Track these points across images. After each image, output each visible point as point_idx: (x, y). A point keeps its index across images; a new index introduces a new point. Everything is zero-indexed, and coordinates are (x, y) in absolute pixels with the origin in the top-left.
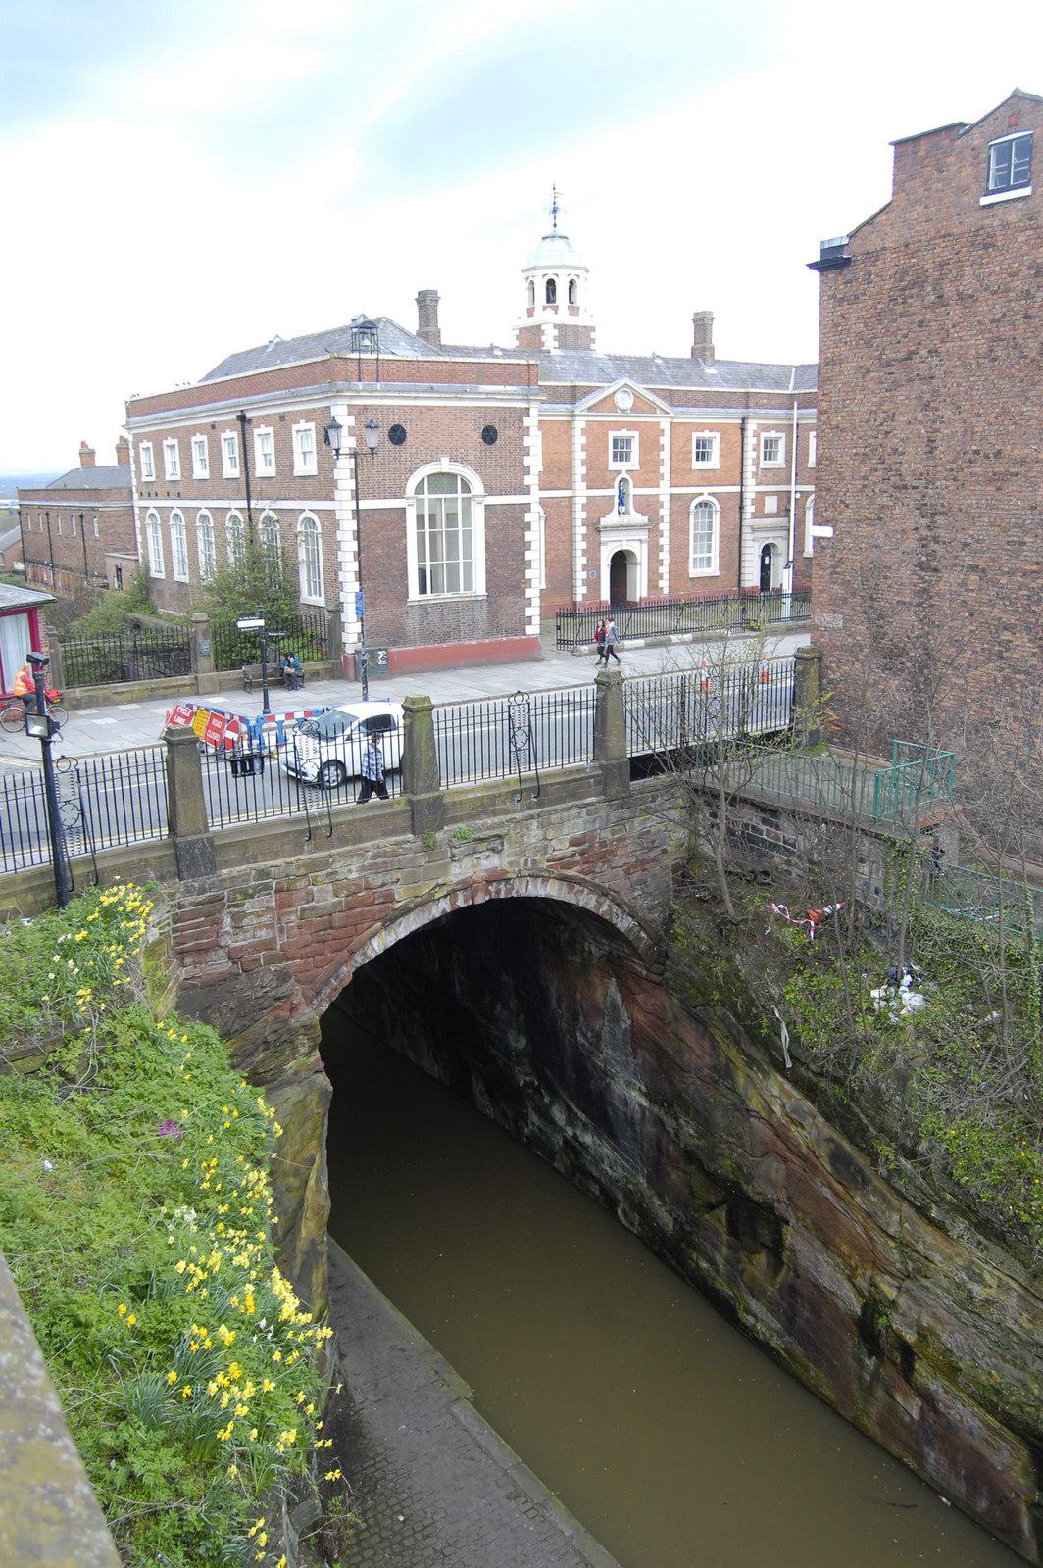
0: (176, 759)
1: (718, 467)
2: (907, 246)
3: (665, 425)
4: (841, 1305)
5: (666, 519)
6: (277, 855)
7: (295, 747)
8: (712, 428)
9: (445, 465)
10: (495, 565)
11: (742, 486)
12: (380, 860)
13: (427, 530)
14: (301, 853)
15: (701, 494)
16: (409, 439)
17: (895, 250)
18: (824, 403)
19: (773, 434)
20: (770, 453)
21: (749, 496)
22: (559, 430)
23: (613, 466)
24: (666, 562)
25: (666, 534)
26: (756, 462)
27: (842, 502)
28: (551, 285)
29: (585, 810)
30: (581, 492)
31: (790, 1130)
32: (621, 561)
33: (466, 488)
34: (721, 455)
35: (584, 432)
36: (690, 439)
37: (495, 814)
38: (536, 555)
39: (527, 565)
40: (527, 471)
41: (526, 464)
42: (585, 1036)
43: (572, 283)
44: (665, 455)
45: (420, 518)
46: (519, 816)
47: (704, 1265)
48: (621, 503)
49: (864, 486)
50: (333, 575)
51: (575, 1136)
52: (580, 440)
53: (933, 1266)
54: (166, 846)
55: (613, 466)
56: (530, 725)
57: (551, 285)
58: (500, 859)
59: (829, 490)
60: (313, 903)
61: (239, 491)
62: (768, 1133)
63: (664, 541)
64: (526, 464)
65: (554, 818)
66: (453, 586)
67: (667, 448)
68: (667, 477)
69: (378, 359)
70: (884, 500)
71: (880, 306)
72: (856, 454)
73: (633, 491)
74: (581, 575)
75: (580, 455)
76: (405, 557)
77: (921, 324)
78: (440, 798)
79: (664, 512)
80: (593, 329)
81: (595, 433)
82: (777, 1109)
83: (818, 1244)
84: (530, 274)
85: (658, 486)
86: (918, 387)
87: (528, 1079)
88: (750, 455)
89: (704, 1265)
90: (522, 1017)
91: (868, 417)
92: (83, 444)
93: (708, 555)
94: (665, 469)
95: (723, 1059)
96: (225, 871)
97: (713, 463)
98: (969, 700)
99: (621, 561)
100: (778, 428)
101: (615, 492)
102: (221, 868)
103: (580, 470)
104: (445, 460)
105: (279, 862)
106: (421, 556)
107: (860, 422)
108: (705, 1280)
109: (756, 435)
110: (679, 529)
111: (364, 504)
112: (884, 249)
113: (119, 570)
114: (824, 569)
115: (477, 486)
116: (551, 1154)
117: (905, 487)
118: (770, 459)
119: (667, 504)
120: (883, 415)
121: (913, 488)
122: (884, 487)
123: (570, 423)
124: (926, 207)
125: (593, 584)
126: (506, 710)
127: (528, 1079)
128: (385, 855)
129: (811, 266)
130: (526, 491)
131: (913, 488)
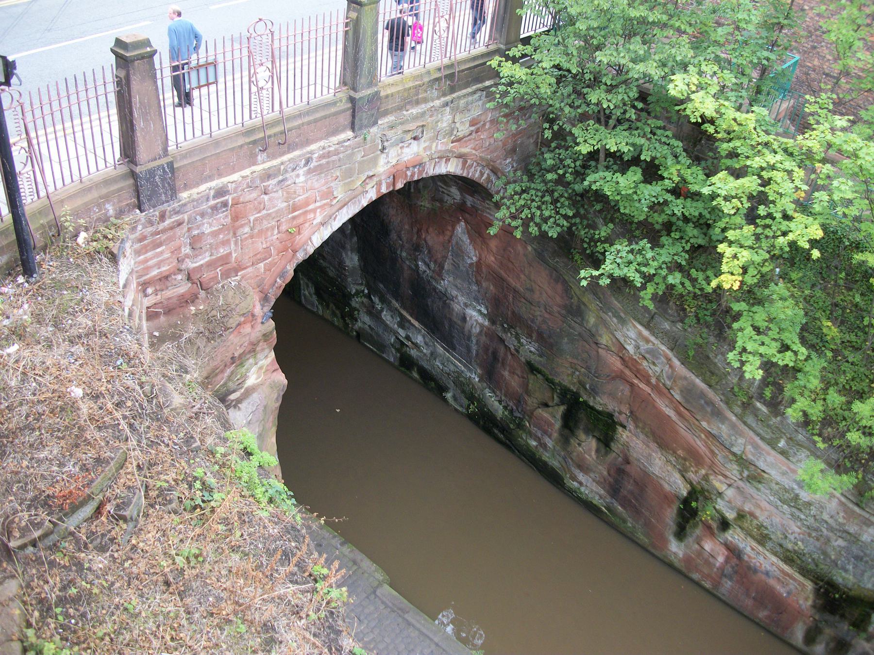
0: (133, 78)
4: (666, 486)
6: (234, 171)
12: (324, 161)
14: (255, 163)
31: (641, 365)
37: (418, 103)
42: (428, 266)
46: (437, 103)
47: (534, 443)
51: (408, 338)
53: (766, 475)
54: (123, 177)
58: (418, 145)
60: (264, 212)
62: (617, 364)
65: (462, 102)
78: (377, 93)
82: (630, 348)
83: (653, 446)
87: (359, 288)
89: (534, 443)
90: (355, 239)
95: (575, 301)
98: (806, 7)
102: (180, 191)
105: (235, 177)
108: (534, 454)
116: (382, 347)
127: (359, 288)
128: (328, 155)
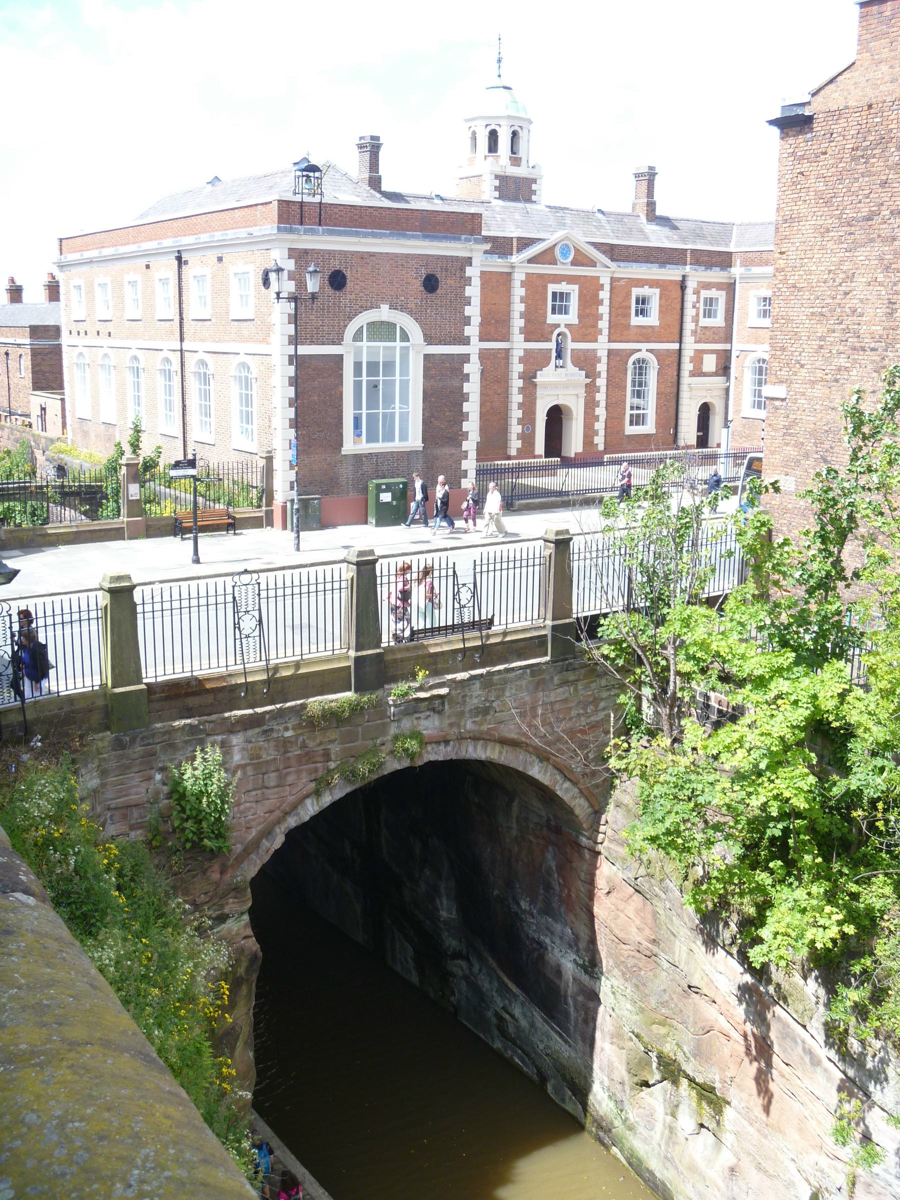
1: (657, 323)
2: (870, 107)
3: (605, 281)
5: (604, 375)
7: (234, 598)
8: (653, 284)
9: (384, 313)
10: (432, 416)
11: (681, 342)
13: (364, 378)
15: (640, 350)
16: (349, 284)
17: (859, 110)
18: (781, 262)
19: (713, 293)
20: (710, 310)
21: (688, 354)
22: (497, 281)
23: (552, 319)
24: (603, 418)
25: (603, 389)
26: (696, 320)
27: (798, 362)
28: (493, 136)
29: (528, 671)
30: (518, 345)
32: (556, 416)
33: (405, 337)
34: (660, 312)
35: (523, 284)
36: (629, 294)
38: (472, 407)
39: (464, 417)
40: (467, 321)
41: (466, 314)
43: (515, 134)
44: (604, 309)
45: (358, 366)
48: (559, 356)
49: (821, 347)
50: (267, 421)
52: (518, 292)
55: (552, 319)
56: (260, 610)
57: (493, 136)
59: (783, 349)
61: (172, 333)
63: (601, 397)
64: (466, 314)
66: (389, 437)
67: (607, 302)
68: (606, 332)
69: (320, 203)
70: (842, 361)
71: (841, 165)
72: (813, 314)
73: (571, 345)
74: (515, 429)
75: (518, 308)
76: (341, 405)
77: (884, 184)
79: (602, 367)
80: (534, 181)
81: (536, 285)
84: (472, 124)
85: (596, 341)
86: (878, 248)
88: (689, 312)
91: (826, 276)
92: (12, 280)
93: (632, 412)
94: (604, 324)
96: (158, 725)
97: (652, 320)
99: (556, 416)
100: (719, 286)
101: (552, 345)
103: (518, 323)
104: (385, 307)
106: (358, 405)
107: (818, 281)
109: (697, 292)
110: (615, 384)
111: (304, 350)
112: (847, 108)
113: (43, 409)
114: (776, 430)
115: (416, 332)
117: (863, 349)
118: (710, 317)
119: (604, 360)
120: (842, 276)
121: (872, 350)
122: (841, 348)
123: (510, 274)
124: (891, 67)
125: (528, 439)
126: (229, 590)
129: (771, 122)
130: (466, 341)
131: (872, 350)
